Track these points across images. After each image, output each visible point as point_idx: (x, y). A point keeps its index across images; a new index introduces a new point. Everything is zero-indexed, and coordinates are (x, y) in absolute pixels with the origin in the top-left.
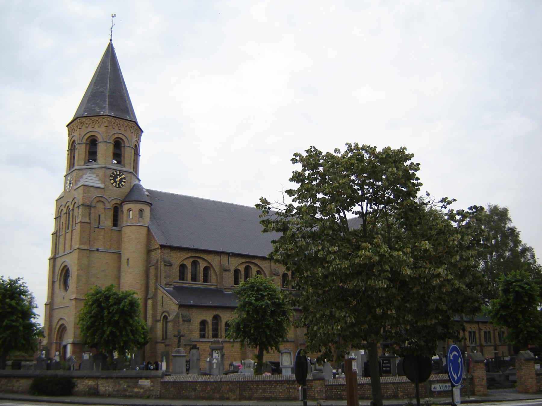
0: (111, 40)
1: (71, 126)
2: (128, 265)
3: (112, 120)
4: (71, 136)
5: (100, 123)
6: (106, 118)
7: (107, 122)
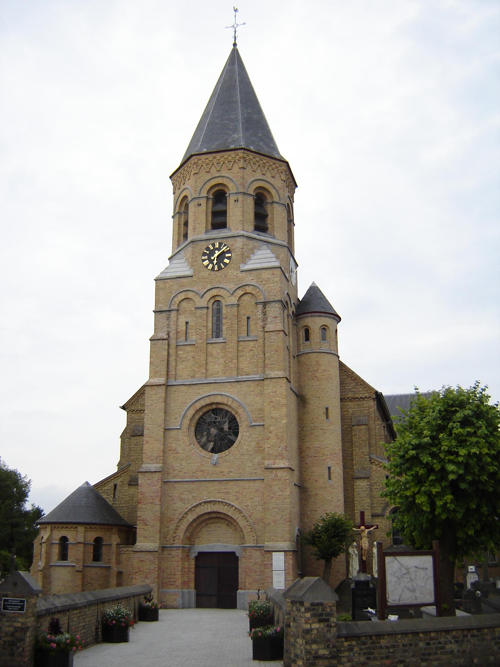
0: (235, 45)
1: (179, 175)
2: (327, 418)
3: (233, 156)
4: (178, 192)
5: (209, 166)
6: (240, 153)
7: (242, 160)
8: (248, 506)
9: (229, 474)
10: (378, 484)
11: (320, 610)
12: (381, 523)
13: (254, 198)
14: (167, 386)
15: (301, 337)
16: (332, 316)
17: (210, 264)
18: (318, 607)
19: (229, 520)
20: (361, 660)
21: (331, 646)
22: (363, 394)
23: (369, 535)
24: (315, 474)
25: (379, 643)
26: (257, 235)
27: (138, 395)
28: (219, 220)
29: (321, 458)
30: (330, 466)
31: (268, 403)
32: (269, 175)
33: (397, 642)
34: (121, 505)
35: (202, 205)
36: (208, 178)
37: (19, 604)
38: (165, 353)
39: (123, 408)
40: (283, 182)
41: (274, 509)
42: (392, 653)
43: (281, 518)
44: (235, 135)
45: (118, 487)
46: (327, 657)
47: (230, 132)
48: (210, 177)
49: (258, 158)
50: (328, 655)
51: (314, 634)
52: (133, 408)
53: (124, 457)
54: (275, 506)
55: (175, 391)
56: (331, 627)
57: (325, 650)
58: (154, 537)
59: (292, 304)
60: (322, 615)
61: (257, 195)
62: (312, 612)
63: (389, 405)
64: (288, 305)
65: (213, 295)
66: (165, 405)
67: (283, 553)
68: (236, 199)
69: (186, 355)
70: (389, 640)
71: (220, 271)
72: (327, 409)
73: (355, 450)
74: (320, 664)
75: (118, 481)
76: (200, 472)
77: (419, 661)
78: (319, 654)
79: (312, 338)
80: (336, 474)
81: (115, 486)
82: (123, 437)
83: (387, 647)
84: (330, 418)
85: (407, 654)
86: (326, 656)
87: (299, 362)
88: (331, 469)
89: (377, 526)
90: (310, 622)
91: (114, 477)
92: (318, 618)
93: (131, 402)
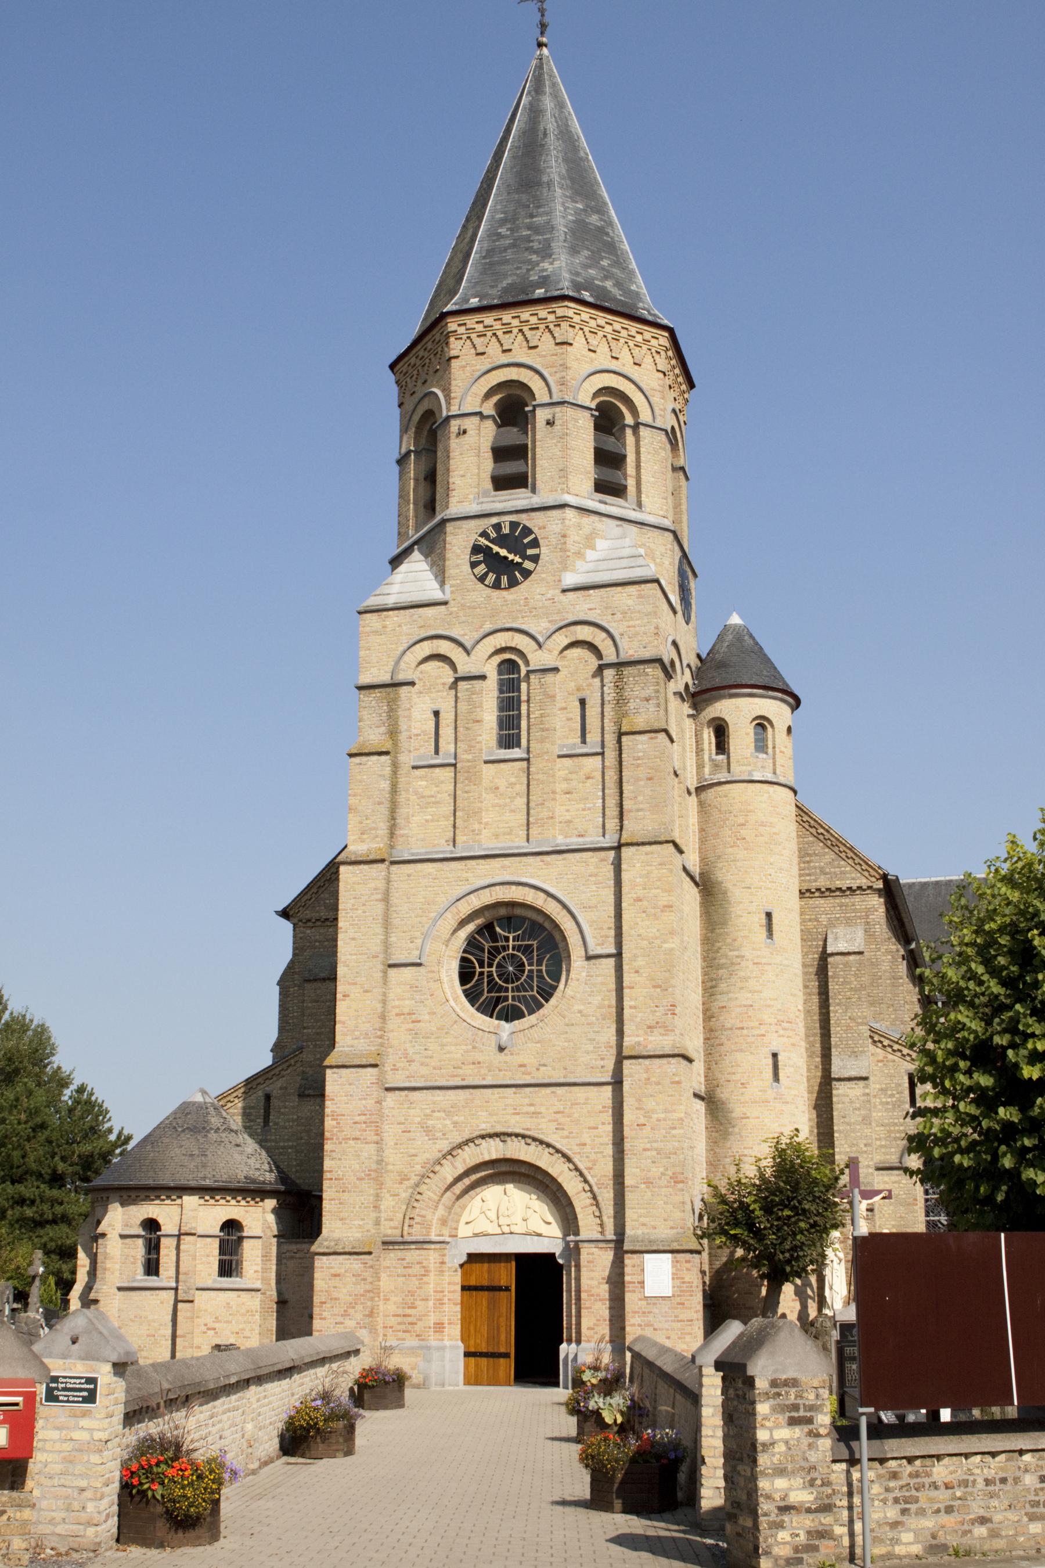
8: (585, 1144)
9: (538, 1069)
10: (889, 1092)
11: (793, 1397)
12: (896, 1185)
13: (592, 415)
14: (618, 848)
15: (706, 746)
16: (780, 695)
17: (491, 574)
18: (787, 1389)
19: (540, 1177)
20: (888, 1515)
21: (819, 1482)
22: (853, 879)
23: (869, 1213)
24: (740, 1070)
25: (928, 1475)
26: (601, 502)
27: (319, 884)
28: (511, 468)
29: (758, 1032)
30: (775, 1050)
31: (632, 901)
32: (625, 356)
33: (973, 1474)
34: (282, 1144)
35: (470, 432)
36: (485, 368)
37: (83, 1386)
38: (385, 785)
39: (285, 914)
40: (661, 375)
41: (649, 1153)
42: (960, 1499)
43: (663, 1174)
44: (545, 265)
45: (274, 1102)
46: (810, 1508)
47: (534, 257)
48: (489, 366)
49: (602, 318)
50: (812, 1503)
51: (779, 1453)
52: (308, 914)
53: (288, 1031)
54: (648, 1146)
55: (409, 876)
56: (818, 1435)
57: (805, 1492)
58: (363, 1220)
59: (685, 665)
60: (795, 1407)
61: (599, 407)
62: (772, 1402)
63: (911, 903)
64: (674, 670)
65: (499, 647)
66: (387, 909)
67: (669, 1255)
68: (550, 417)
69: (435, 789)
70: (951, 1468)
71: (512, 590)
72: (769, 915)
73: (836, 1012)
74: (794, 1524)
75: (275, 1087)
76: (472, 1066)
77: (1025, 1519)
78: (792, 1500)
79: (731, 748)
80: (792, 1070)
81: (268, 1097)
82: (284, 983)
83: (948, 1486)
84: (775, 936)
85: (995, 1503)
86: (807, 1505)
87: (701, 804)
88: (780, 1058)
89: (890, 1191)
90: (767, 1424)
91: (264, 1077)
92: (788, 1414)
93: (303, 900)
